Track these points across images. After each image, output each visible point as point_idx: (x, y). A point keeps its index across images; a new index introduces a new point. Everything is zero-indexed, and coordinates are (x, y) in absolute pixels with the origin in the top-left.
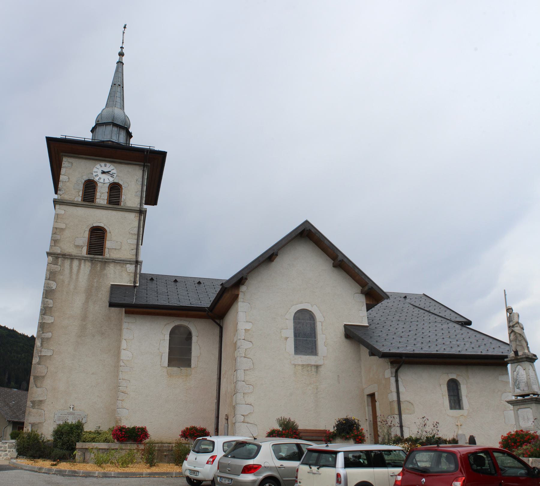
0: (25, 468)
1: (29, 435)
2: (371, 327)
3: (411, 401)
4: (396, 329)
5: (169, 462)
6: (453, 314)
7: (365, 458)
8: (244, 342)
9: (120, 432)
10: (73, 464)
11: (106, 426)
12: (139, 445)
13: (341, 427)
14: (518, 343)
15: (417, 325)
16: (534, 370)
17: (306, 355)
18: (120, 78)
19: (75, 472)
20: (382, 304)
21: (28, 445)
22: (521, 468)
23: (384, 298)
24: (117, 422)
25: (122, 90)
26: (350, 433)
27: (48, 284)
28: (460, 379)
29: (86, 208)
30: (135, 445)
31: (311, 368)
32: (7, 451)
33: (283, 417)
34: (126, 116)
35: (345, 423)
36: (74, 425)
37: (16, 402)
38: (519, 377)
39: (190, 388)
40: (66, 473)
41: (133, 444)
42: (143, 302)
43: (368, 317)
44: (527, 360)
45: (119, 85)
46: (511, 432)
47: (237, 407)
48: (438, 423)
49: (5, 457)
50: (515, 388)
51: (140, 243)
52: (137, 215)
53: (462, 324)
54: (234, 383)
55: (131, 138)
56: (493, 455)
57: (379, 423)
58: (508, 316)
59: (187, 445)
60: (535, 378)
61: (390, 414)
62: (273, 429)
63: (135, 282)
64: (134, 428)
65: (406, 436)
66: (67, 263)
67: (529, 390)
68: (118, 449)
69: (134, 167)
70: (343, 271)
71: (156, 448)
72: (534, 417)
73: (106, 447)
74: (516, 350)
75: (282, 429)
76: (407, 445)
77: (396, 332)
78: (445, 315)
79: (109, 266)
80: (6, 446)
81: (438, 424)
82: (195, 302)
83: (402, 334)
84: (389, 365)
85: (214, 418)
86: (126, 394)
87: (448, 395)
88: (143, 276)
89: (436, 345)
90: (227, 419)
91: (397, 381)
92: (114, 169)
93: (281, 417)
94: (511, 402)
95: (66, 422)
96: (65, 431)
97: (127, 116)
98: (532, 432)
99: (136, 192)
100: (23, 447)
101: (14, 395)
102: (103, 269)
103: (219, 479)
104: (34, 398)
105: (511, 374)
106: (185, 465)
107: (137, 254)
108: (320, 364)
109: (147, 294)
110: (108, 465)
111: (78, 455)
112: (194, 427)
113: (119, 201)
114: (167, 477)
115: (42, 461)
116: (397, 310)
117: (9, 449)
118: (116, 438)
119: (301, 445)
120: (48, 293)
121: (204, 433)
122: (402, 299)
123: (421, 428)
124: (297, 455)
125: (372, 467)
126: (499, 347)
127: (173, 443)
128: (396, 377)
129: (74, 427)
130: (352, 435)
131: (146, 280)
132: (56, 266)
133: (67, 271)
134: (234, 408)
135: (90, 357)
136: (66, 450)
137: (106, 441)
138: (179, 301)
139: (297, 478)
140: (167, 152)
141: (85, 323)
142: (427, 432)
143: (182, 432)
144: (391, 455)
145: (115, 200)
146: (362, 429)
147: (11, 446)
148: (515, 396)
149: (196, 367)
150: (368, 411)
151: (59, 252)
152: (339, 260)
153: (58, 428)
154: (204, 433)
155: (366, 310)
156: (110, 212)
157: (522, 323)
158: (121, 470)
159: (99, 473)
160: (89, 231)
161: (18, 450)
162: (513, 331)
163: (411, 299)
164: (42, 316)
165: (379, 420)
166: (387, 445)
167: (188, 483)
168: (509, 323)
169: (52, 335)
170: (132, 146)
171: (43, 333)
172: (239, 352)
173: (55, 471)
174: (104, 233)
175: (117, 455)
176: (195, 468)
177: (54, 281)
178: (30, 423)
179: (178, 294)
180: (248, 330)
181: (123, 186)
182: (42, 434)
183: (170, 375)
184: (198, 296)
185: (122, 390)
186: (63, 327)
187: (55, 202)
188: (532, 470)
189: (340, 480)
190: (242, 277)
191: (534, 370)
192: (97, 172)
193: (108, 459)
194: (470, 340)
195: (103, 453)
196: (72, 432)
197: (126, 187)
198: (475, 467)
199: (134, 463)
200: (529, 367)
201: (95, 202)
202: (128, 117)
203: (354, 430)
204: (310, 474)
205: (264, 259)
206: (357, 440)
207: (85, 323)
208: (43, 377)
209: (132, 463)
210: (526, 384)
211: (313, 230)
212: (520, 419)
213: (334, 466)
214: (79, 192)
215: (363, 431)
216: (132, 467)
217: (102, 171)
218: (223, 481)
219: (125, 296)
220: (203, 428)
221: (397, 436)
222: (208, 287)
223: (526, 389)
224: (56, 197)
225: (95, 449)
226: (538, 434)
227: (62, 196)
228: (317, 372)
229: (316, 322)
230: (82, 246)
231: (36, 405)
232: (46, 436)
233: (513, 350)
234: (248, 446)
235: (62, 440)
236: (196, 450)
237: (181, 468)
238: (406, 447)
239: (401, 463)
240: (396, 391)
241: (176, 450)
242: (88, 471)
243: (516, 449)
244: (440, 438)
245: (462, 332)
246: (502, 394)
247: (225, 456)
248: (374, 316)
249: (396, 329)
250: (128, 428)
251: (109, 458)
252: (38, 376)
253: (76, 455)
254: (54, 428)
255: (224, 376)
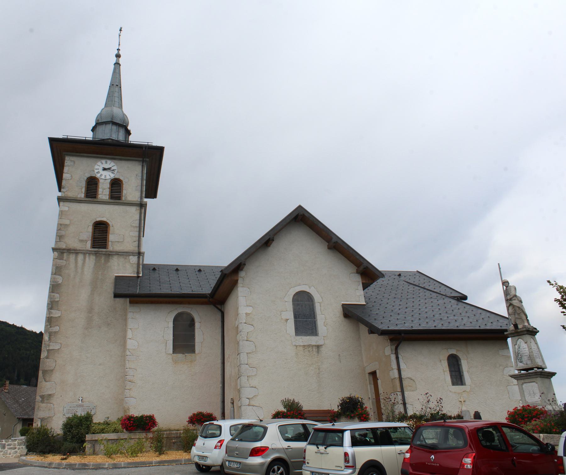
0: (35, 465)
1: (39, 430)
2: (367, 306)
3: (413, 378)
4: (393, 306)
5: (178, 449)
6: (448, 289)
7: (372, 436)
8: (246, 326)
9: (128, 422)
10: (82, 457)
11: (115, 416)
12: (148, 433)
13: (345, 406)
14: (517, 316)
15: (413, 302)
16: (536, 344)
17: (307, 336)
18: (117, 79)
19: (85, 465)
20: (377, 282)
21: (38, 440)
22: (534, 445)
23: (379, 277)
24: (125, 411)
25: (119, 90)
26: (355, 411)
27: (54, 278)
28: (460, 355)
29: (89, 204)
30: (144, 433)
31: (312, 349)
32: (17, 448)
33: (287, 399)
34: (124, 115)
35: (349, 402)
36: (83, 417)
37: (25, 398)
38: (520, 350)
39: (195, 374)
40: (76, 466)
41: (141, 433)
42: (146, 291)
43: (364, 296)
44: (528, 333)
45: (117, 85)
46: (517, 407)
47: (242, 390)
48: (442, 399)
49: (15, 455)
50: (518, 362)
51: (142, 235)
52: (138, 208)
53: (458, 299)
54: (237, 367)
55: (130, 135)
56: (502, 430)
57: (382, 401)
58: (505, 289)
59: (195, 431)
60: (538, 351)
61: (393, 392)
62: (278, 411)
63: (138, 273)
64: (142, 417)
65: (410, 413)
66: (72, 257)
67: (532, 363)
68: (127, 439)
69: (134, 163)
70: (338, 252)
71: (165, 436)
72: (540, 391)
73: (116, 438)
74: (515, 323)
75: (287, 411)
76: (412, 423)
77: (393, 309)
78: (440, 291)
79: (113, 258)
80: (16, 444)
81: (441, 400)
82: (197, 290)
83: (399, 312)
84: (389, 342)
85: (220, 403)
86: (133, 383)
87: (449, 371)
88: (145, 267)
89: (434, 321)
90: (233, 403)
91: (397, 358)
92: (114, 166)
93: (285, 399)
94: (514, 377)
95: (75, 414)
96: (74, 424)
97: (126, 115)
98: (540, 407)
99: (137, 187)
100: (33, 443)
101: (24, 392)
102: (107, 261)
103: (227, 463)
104: (43, 392)
105: (513, 348)
106: (193, 451)
107: (139, 246)
108: (321, 344)
109: (150, 284)
110: (117, 455)
111: (87, 447)
112: (201, 413)
113: (120, 196)
114: (176, 464)
115: (53, 456)
116: (392, 287)
117: (18, 447)
118: (125, 428)
119: (307, 425)
120: (54, 288)
121: (210, 417)
122: (396, 277)
123: (425, 404)
124: (303, 436)
125: (380, 445)
126: (498, 320)
127: (181, 430)
128: (397, 354)
129: (83, 419)
130: (357, 413)
131: (148, 271)
132: (61, 261)
133: (72, 265)
134: (239, 391)
135: (96, 348)
136: (75, 444)
137: (115, 431)
138: (181, 289)
139: (304, 458)
140: (164, 147)
141: (91, 315)
142: (431, 409)
143: (189, 418)
144: (396, 433)
145: (116, 194)
146: (366, 408)
147: (20, 443)
148: (518, 370)
149: (200, 352)
150: (371, 389)
151: (64, 247)
152: (333, 242)
153: (67, 421)
154: (210, 417)
155: (362, 289)
156: (112, 206)
157: (519, 296)
158: (130, 460)
159: (109, 464)
160: (93, 226)
161: (27, 447)
162: (511, 304)
163: (405, 276)
164: (49, 311)
165: (381, 397)
166: (392, 422)
167: (197, 469)
168: (507, 296)
169: (59, 329)
170: (131, 142)
171: (51, 327)
172: (241, 335)
173: (66, 465)
174: (107, 227)
175: (126, 445)
176: (204, 453)
177: (60, 275)
178: (39, 418)
179: (180, 283)
180: (249, 314)
181: (124, 182)
182: (51, 429)
183: (175, 362)
184: (199, 283)
185: (129, 379)
186: (70, 320)
187: (59, 200)
188: (545, 446)
189: (348, 459)
190: (241, 263)
191: (536, 344)
192: (98, 169)
193: (117, 450)
194: (468, 315)
195: (113, 443)
196: (81, 424)
197: (126, 182)
198: (484, 443)
199: (144, 452)
200: (531, 340)
201: (98, 198)
202: (126, 116)
203: (358, 408)
204: (317, 454)
205: (261, 244)
206: (361, 418)
207: (91, 315)
208: (52, 370)
209: (141, 453)
210: (528, 357)
211: (306, 215)
212: (526, 393)
213: (341, 445)
214: (82, 189)
215: (367, 409)
216: (141, 457)
217: (103, 168)
218: (232, 465)
219: (129, 287)
220: (210, 413)
221: (402, 413)
222: (209, 274)
223: (529, 362)
224: (60, 194)
225: (105, 440)
226: (547, 410)
227: (66, 193)
228: (318, 352)
229: (315, 303)
230: (86, 240)
231: (45, 399)
232: (56, 430)
233: (512, 323)
234: (255, 428)
235: (72, 433)
236: (204, 435)
237: (190, 455)
238: (411, 424)
239: (408, 440)
240: (397, 368)
241: (184, 436)
242: (98, 463)
243: (525, 424)
244: (444, 414)
245: (458, 307)
246: (504, 369)
247: (233, 440)
248: (370, 294)
249: (393, 306)
250: (136, 417)
251: (118, 448)
252: (47, 370)
253: (86, 447)
254: (63, 422)
255: (227, 360)
